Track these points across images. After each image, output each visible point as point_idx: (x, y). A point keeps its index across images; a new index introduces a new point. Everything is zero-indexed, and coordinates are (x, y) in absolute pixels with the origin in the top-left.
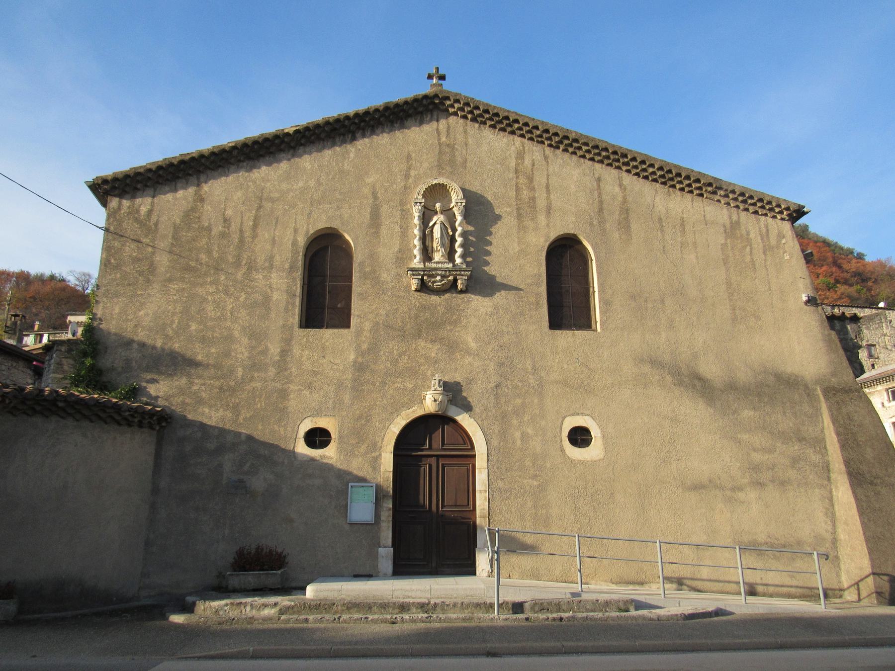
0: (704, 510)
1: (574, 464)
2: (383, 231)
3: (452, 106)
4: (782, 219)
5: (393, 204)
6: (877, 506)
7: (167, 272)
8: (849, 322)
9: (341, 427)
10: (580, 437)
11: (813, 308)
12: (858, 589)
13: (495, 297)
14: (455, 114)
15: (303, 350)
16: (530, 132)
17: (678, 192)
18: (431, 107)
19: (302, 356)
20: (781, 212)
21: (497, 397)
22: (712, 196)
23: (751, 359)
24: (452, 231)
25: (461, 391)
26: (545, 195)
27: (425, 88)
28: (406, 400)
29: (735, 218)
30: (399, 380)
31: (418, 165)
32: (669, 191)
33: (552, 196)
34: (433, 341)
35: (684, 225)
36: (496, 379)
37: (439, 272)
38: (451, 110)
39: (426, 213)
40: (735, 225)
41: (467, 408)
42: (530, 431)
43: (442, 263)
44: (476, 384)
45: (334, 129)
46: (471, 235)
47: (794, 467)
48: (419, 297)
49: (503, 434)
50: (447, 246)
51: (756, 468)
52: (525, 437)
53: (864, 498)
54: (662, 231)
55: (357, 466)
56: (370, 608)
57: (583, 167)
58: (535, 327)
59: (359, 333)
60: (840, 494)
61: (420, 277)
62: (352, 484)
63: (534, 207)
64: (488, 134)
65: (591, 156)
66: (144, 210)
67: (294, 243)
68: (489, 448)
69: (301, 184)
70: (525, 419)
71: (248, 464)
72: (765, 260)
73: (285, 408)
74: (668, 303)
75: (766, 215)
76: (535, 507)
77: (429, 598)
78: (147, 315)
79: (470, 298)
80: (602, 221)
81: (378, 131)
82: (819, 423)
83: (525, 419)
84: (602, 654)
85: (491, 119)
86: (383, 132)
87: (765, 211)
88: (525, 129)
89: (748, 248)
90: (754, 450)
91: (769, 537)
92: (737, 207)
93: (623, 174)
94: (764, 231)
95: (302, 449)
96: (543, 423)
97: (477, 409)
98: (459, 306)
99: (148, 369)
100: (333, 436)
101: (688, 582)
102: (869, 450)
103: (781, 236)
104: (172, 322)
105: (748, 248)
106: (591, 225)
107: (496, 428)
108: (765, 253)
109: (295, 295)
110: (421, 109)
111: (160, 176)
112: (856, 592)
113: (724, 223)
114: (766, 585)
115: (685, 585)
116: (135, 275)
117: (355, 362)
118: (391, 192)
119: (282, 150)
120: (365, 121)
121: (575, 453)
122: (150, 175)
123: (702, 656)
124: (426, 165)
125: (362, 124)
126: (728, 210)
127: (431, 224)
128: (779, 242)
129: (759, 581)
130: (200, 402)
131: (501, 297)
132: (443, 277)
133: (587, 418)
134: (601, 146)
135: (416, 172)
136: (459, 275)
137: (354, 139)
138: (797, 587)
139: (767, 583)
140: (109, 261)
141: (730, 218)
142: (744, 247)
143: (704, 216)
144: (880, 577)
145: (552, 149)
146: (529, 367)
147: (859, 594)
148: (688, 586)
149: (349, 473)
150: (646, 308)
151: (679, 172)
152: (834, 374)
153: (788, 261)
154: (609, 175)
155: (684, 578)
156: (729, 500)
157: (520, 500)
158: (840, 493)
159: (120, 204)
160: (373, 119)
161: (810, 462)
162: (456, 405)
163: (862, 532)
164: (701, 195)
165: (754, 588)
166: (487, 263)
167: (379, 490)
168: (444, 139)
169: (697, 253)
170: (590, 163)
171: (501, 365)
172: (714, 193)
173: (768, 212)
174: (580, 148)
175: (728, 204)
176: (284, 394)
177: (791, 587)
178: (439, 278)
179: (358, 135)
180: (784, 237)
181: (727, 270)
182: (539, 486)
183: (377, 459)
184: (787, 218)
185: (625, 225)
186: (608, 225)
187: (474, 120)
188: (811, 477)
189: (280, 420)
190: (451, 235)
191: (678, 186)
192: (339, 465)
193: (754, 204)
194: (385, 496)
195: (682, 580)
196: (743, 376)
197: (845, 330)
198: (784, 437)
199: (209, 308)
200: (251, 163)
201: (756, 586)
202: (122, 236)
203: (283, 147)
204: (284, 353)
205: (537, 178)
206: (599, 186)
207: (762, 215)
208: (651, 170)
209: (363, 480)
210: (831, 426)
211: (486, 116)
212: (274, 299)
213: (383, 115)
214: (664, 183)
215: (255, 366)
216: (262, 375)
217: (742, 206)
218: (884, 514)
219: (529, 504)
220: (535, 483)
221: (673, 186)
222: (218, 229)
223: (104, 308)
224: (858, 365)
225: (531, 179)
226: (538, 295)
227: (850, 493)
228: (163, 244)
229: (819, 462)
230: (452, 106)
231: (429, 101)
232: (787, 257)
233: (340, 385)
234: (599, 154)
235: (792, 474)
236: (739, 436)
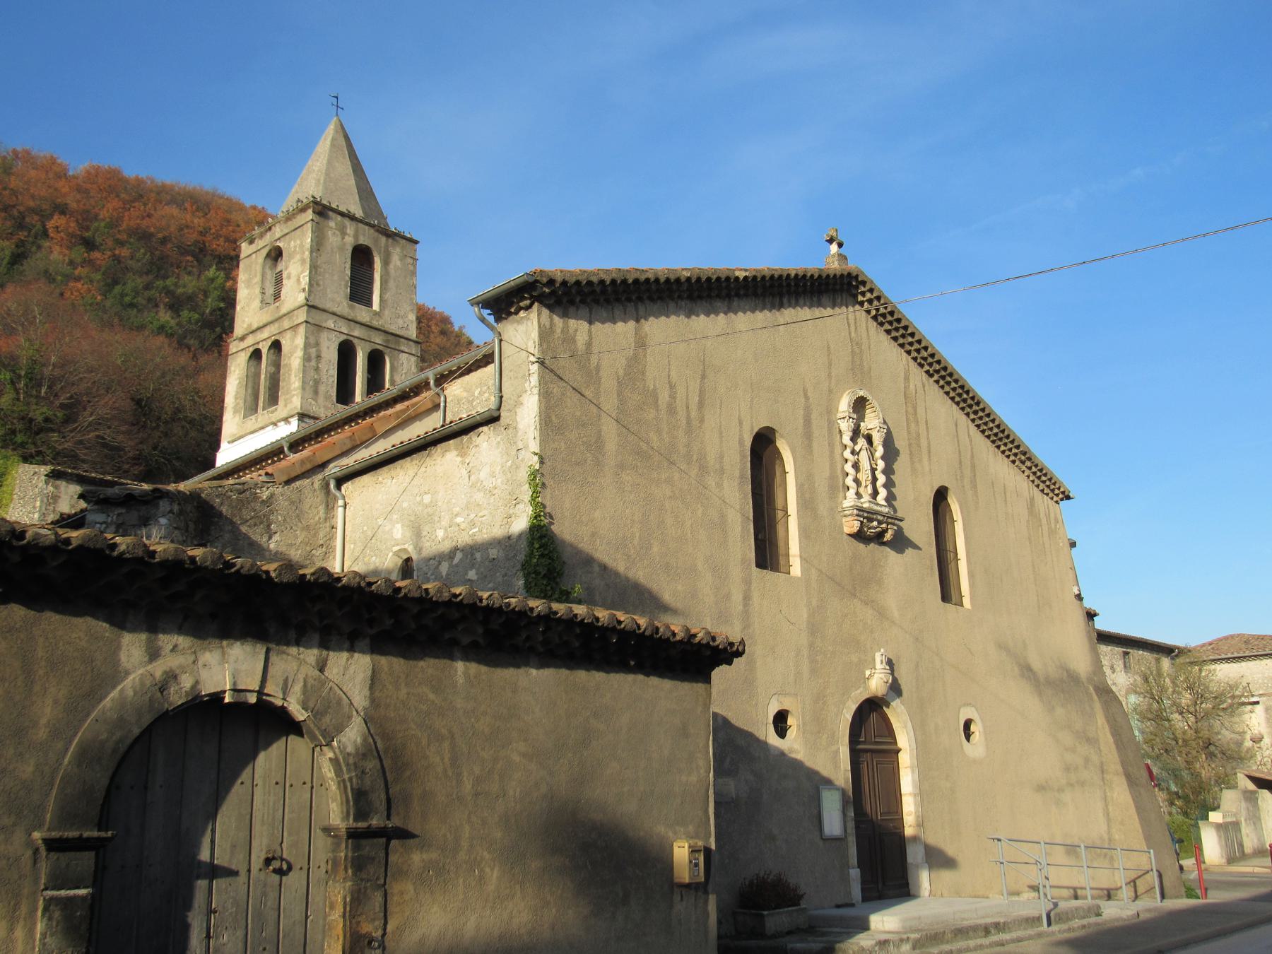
2: (815, 445)
3: (863, 294)
12: (1135, 887)
14: (862, 304)
16: (918, 351)
27: (828, 260)
37: (879, 517)
38: (860, 298)
43: (881, 505)
60: (1115, 795)
66: (581, 339)
67: (741, 443)
68: (765, 710)
71: (728, 760)
85: (891, 323)
86: (805, 305)
88: (916, 346)
109: (748, 518)
112: (1133, 889)
116: (582, 448)
147: (1136, 891)
158: (1116, 793)
163: (1140, 831)
167: (844, 792)
170: (950, 401)
174: (949, 383)
175: (1028, 477)
178: (875, 523)
191: (1003, 448)
210: (1106, 726)
211: (889, 318)
222: (664, 397)
227: (1127, 793)
230: (863, 294)
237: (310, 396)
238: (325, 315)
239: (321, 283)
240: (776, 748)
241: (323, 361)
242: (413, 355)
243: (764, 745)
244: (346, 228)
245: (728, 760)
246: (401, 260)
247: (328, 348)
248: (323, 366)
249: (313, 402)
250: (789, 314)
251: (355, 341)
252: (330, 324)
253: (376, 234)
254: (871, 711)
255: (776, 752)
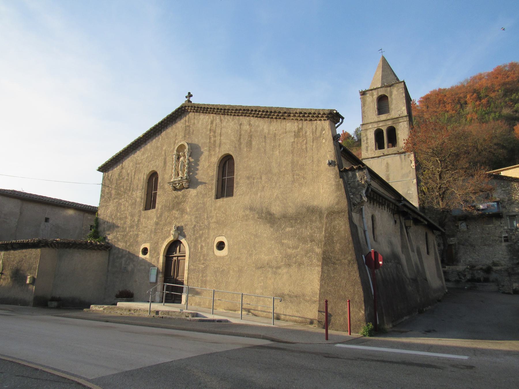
0: (262, 278)
1: (217, 258)
4: (325, 120)
6: (332, 276)
7: (114, 196)
8: (358, 171)
9: (151, 246)
10: (221, 246)
11: (332, 168)
13: (198, 188)
14: (190, 112)
15: (143, 219)
17: (275, 120)
18: (183, 111)
20: (322, 117)
21: (194, 231)
22: (289, 118)
23: (297, 201)
25: (183, 230)
26: (219, 138)
28: (168, 235)
29: (300, 126)
30: (166, 227)
32: (271, 120)
33: (222, 138)
34: (177, 210)
35: (275, 137)
36: (194, 223)
40: (300, 130)
41: (184, 236)
42: (204, 245)
44: (188, 226)
45: (155, 131)
46: (193, 163)
47: (306, 256)
49: (195, 246)
51: (289, 257)
52: (202, 247)
53: (326, 271)
54: (265, 142)
55: (153, 261)
56: (122, 310)
57: (235, 120)
58: (209, 199)
59: (157, 210)
61: (172, 185)
62: (152, 268)
63: (215, 145)
64: (202, 116)
65: (237, 114)
69: (146, 156)
70: (203, 240)
71: (128, 262)
72: (313, 146)
73: (138, 241)
74: (264, 178)
75: (316, 120)
76: (202, 276)
78: (109, 212)
79: (190, 190)
80: (240, 144)
81: (168, 127)
82: (323, 232)
83: (203, 240)
87: (315, 119)
89: (305, 140)
90: (289, 248)
91: (290, 291)
92: (302, 120)
93: (251, 118)
94: (314, 129)
95: (141, 255)
96: (208, 241)
97: (187, 237)
98: (186, 194)
99: (108, 230)
100: (149, 250)
101: (252, 311)
102: (338, 245)
103: (323, 129)
104: (114, 214)
105: (305, 140)
106: (235, 147)
107: (193, 244)
108: (313, 142)
110: (180, 114)
111: (113, 163)
113: (295, 130)
114: (285, 315)
115: (251, 313)
117: (156, 221)
119: (142, 144)
120: (162, 125)
121: (218, 253)
122: (110, 163)
123: (127, 326)
124: (181, 137)
125: (163, 126)
126: (297, 122)
128: (321, 133)
129: (282, 313)
130: (118, 240)
131: (200, 188)
132: (179, 183)
133: (224, 237)
134: (238, 108)
136: (183, 182)
137: (161, 133)
138: (299, 317)
139: (286, 314)
140: (102, 195)
141: (298, 127)
142: (303, 141)
143: (286, 129)
144: (322, 313)
145: (224, 115)
146: (206, 217)
148: (252, 313)
149: (151, 264)
150: (253, 182)
151: (271, 111)
152: (337, 204)
153: (324, 143)
154: (244, 120)
155: (251, 309)
156: (275, 273)
157: (198, 273)
159: (105, 174)
160: (165, 123)
161: (315, 253)
162: (181, 236)
164: (284, 119)
165: (279, 316)
166: (196, 174)
168: (187, 124)
169: (279, 150)
171: (196, 217)
172: (289, 116)
173: (316, 118)
176: (137, 235)
177: (297, 317)
179: (162, 131)
180: (324, 130)
181: (293, 155)
182: (204, 267)
183: (159, 258)
184: (326, 119)
185: (249, 144)
186: (242, 146)
187: (197, 112)
188: (314, 261)
189: (136, 245)
192: (149, 261)
193: (308, 116)
194: (160, 272)
195: (250, 310)
196: (291, 211)
197: (355, 176)
198: (303, 240)
199: (122, 207)
200: (135, 151)
201: (281, 315)
202: (105, 186)
203: (142, 142)
204: (139, 220)
205: (217, 131)
206: (240, 127)
207: (314, 121)
208: (260, 113)
209: (154, 266)
212: (137, 201)
213: (168, 121)
214: (268, 118)
215: (132, 227)
216: (133, 229)
217: (303, 118)
218: (335, 280)
219: (201, 275)
220: (203, 266)
221: (272, 118)
223: (101, 211)
224: (359, 195)
225: (215, 132)
226: (212, 184)
228: (113, 186)
229: (319, 253)
231: (181, 110)
232: (324, 141)
233: (151, 232)
234: (239, 113)
235: (305, 259)
236: (283, 241)
237: (365, 152)
238: (368, 125)
239: (366, 115)
240: (142, 258)
241: (369, 140)
242: (405, 121)
243: (138, 257)
244: (373, 93)
245: (128, 262)
246: (397, 91)
247: (370, 134)
248: (369, 141)
249: (367, 154)
250: (164, 133)
251: (380, 128)
252: (370, 127)
253: (386, 88)
254: (174, 245)
255: (142, 259)
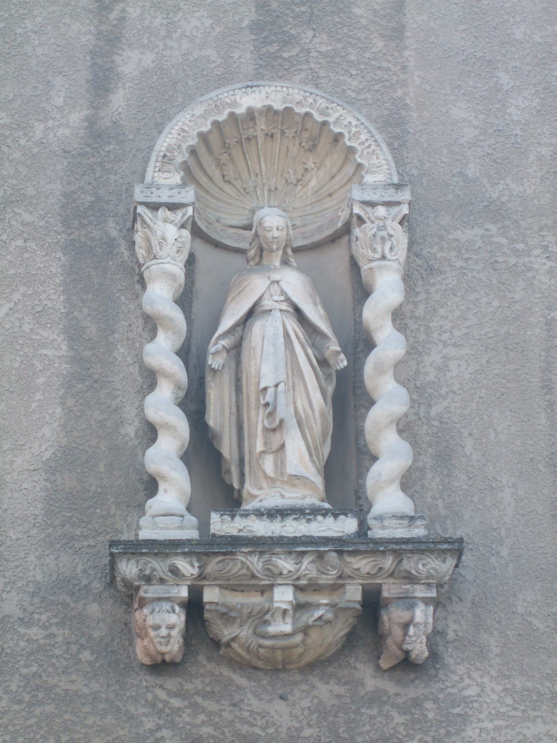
5: (27, 218)
19: (19, 724)
24: (345, 350)
31: (157, 22)
39: (201, 265)
48: (176, 703)
50: (317, 428)
61: (184, 593)
77: (389, 181)
84: (395, 541)
118: (17, 155)
127: (227, 323)
135: (148, 59)
190: (341, 374)
